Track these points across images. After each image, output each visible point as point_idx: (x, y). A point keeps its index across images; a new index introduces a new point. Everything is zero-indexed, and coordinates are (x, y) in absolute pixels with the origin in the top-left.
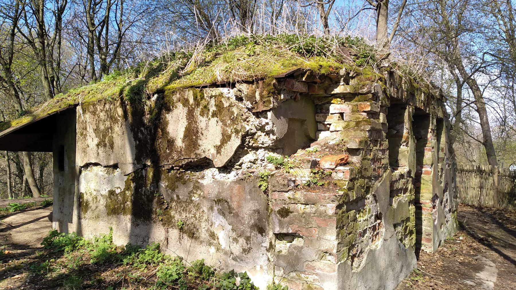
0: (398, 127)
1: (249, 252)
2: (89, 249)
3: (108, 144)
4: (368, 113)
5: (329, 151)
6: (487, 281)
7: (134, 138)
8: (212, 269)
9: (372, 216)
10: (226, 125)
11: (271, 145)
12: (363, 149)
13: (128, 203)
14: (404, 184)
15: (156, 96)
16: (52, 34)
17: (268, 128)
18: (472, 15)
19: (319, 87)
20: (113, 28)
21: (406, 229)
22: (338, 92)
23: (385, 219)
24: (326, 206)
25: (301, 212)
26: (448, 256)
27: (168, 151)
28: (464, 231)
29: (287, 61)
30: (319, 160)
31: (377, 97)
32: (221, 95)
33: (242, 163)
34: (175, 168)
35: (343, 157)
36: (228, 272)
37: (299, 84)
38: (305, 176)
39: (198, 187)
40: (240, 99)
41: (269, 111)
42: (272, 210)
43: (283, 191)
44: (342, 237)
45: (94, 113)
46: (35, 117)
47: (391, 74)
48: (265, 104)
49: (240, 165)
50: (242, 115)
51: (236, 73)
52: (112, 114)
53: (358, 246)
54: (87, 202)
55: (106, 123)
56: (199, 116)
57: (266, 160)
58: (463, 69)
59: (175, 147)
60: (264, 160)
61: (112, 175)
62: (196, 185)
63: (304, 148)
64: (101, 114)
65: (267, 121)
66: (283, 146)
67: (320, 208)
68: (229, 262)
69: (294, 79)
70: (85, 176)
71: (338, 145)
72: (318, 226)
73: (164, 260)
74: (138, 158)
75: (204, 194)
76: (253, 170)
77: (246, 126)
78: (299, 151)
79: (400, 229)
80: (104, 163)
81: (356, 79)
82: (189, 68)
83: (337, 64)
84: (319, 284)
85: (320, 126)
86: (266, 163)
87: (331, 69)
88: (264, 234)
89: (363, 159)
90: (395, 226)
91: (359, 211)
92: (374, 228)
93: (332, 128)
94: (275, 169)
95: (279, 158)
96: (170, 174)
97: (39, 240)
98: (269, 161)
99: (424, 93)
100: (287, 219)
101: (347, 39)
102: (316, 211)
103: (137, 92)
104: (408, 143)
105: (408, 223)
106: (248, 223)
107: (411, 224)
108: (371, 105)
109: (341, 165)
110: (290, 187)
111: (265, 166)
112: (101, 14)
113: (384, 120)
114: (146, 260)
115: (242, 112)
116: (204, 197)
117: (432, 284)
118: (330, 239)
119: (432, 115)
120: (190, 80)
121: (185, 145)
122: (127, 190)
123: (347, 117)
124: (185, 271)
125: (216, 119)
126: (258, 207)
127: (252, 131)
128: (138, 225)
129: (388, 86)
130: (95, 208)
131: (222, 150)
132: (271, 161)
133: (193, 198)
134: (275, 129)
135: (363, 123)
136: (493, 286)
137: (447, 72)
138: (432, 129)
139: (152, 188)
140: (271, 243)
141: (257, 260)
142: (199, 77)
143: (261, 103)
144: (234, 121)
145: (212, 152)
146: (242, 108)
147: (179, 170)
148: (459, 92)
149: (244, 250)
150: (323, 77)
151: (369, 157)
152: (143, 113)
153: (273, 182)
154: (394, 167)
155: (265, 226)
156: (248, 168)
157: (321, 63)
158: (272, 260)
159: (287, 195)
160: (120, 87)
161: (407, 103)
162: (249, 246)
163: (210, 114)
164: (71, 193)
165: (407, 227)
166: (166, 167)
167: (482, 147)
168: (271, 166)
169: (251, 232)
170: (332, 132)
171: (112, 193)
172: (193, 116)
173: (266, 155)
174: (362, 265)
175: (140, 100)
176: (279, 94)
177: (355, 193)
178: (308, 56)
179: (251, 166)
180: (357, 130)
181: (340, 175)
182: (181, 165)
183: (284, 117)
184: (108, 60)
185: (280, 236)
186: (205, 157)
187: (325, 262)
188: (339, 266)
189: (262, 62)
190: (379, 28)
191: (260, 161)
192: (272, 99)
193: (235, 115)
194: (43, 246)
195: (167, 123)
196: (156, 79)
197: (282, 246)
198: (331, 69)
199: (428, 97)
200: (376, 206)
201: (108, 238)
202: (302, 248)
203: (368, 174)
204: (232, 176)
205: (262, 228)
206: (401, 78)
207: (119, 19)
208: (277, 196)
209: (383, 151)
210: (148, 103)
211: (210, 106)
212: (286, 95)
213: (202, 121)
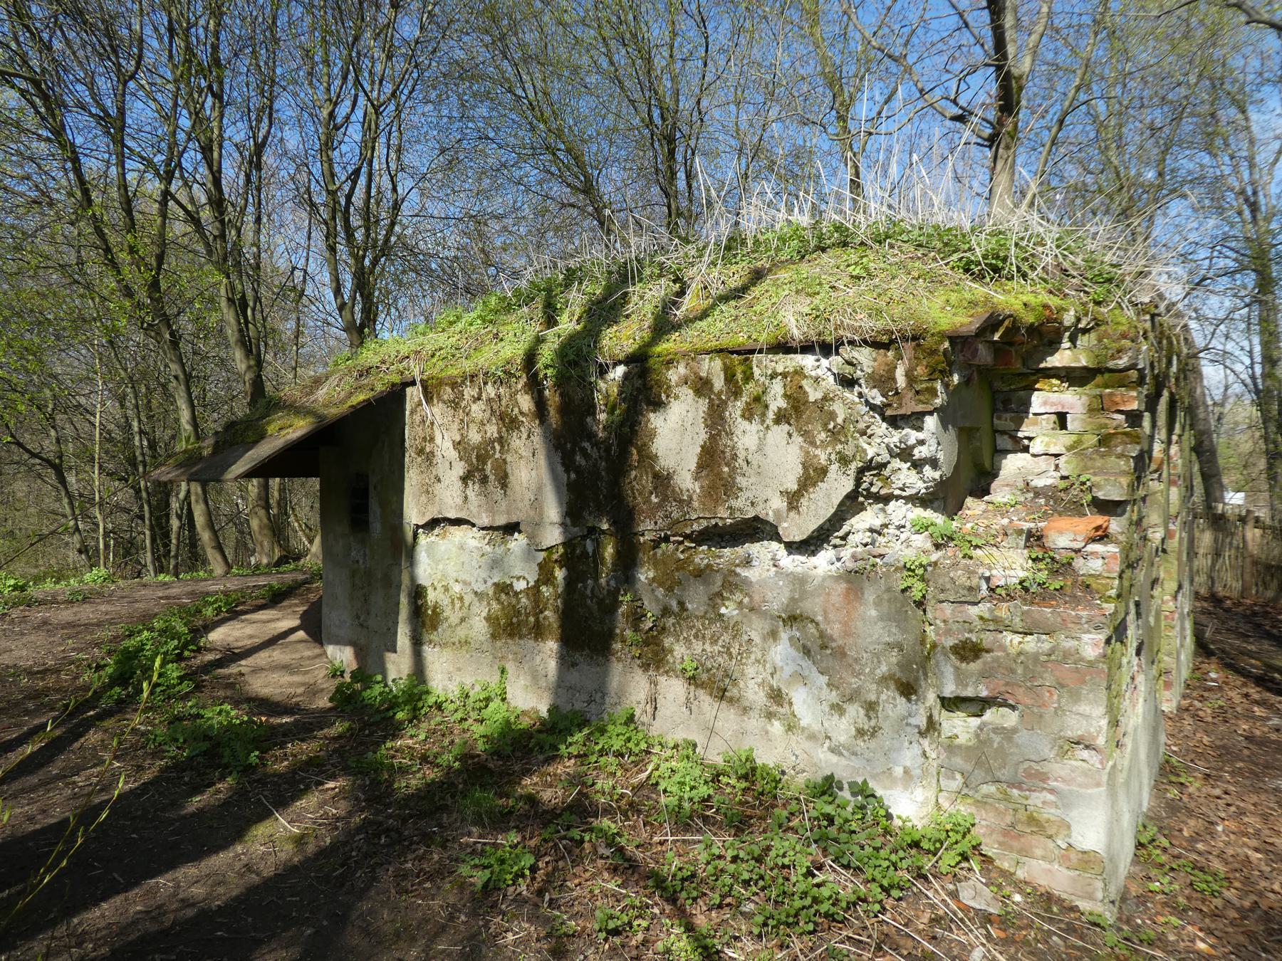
1: (873, 735)
3: (492, 478)
7: (563, 464)
10: (813, 443)
11: (923, 491)
15: (620, 370)
17: (919, 453)
24: (1079, 639)
25: (1013, 651)
26: (1210, 719)
27: (654, 499)
32: (799, 372)
33: (848, 534)
34: (672, 539)
39: (732, 583)
40: (848, 382)
41: (931, 413)
45: (455, 404)
49: (844, 538)
54: (435, 607)
55: (488, 427)
56: (740, 420)
57: (908, 525)
59: (673, 491)
61: (503, 547)
62: (731, 579)
64: (474, 407)
65: (921, 436)
67: (1064, 644)
68: (822, 756)
70: (431, 546)
72: (1059, 684)
74: (573, 513)
76: (881, 551)
80: (485, 520)
81: (1093, 335)
82: (690, 303)
84: (1058, 812)
85: (1003, 442)
88: (914, 697)
93: (1036, 447)
96: (659, 552)
100: (975, 666)
103: (578, 358)
106: (872, 672)
116: (752, 610)
121: (702, 487)
122: (545, 583)
123: (1076, 423)
125: (786, 427)
126: (899, 638)
127: (879, 459)
128: (574, 665)
130: (457, 621)
131: (804, 501)
132: (923, 528)
133: (723, 610)
134: (940, 456)
139: (613, 583)
140: (930, 718)
141: (895, 755)
142: (724, 327)
143: (911, 394)
144: (836, 435)
145: (774, 506)
146: (853, 403)
147: (682, 543)
149: (860, 733)
150: (1032, 329)
152: (591, 409)
153: (941, 581)
155: (917, 679)
158: (934, 755)
159: (974, 611)
162: (873, 723)
163: (771, 415)
164: (391, 585)
168: (921, 541)
169: (879, 693)
171: (503, 588)
172: (722, 418)
173: (911, 516)
181: (1096, 565)
182: (688, 532)
185: (951, 704)
186: (756, 518)
187: (1073, 762)
189: (897, 294)
191: (901, 531)
193: (840, 420)
195: (652, 434)
196: (615, 328)
197: (960, 726)
202: (1014, 730)
204: (823, 562)
210: (602, 384)
211: (768, 398)
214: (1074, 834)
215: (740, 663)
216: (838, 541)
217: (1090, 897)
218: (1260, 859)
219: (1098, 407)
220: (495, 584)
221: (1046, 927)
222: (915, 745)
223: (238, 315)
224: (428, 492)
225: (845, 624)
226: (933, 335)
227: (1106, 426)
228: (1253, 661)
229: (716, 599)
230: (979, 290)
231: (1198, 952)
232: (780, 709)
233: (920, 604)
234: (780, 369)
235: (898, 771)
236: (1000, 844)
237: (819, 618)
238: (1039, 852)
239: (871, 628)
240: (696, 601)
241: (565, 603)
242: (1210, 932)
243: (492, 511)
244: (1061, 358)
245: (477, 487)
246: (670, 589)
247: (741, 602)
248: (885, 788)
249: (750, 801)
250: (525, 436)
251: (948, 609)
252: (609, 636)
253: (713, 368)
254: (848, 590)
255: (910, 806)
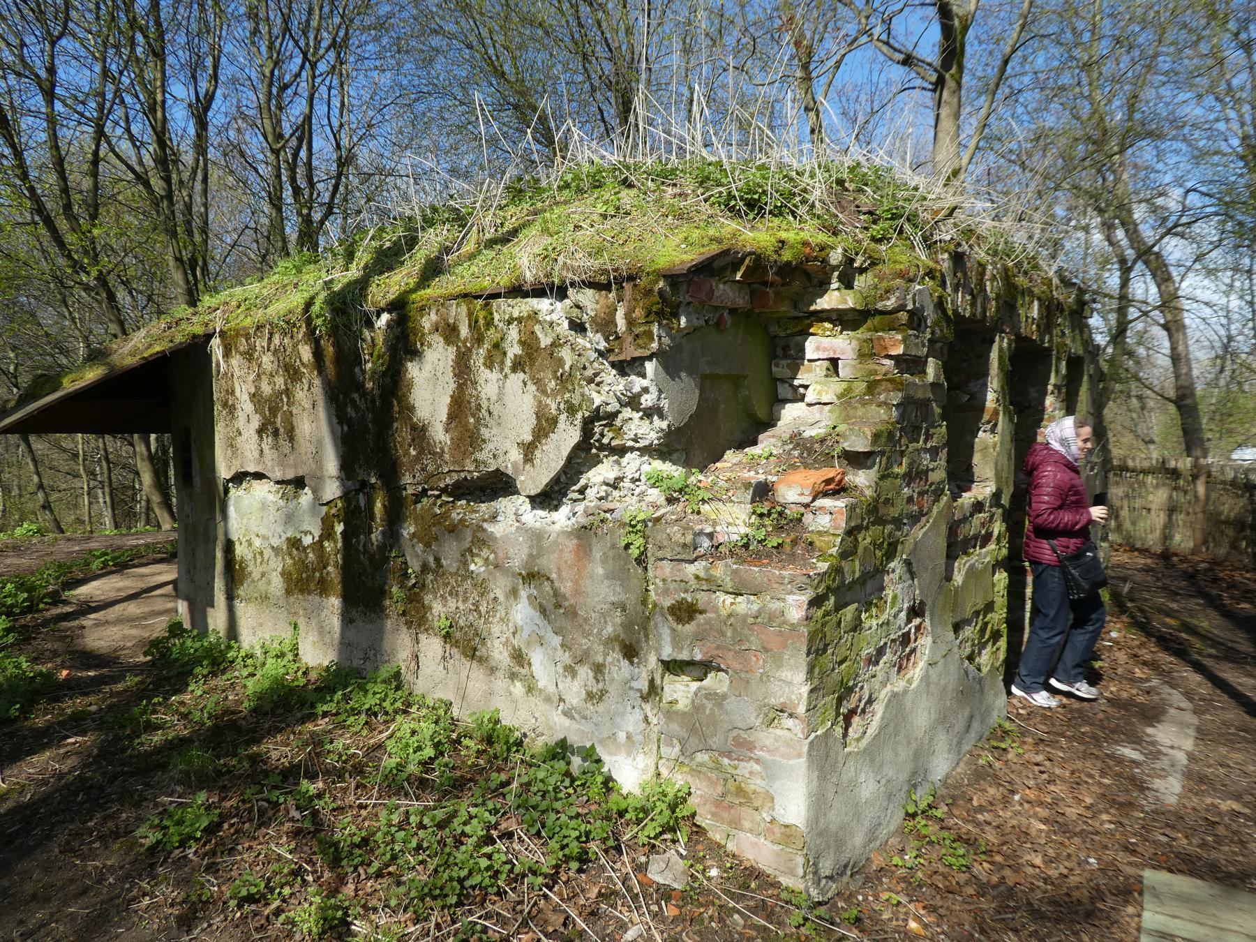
0: (973, 386)
1: (600, 699)
2: (245, 673)
3: (282, 430)
4: (898, 359)
5: (801, 455)
6: (1172, 747)
8: (517, 734)
9: (900, 611)
10: (544, 392)
11: (656, 442)
12: (882, 453)
13: (330, 569)
14: (983, 524)
15: (385, 317)
16: (188, 158)
17: (647, 400)
18: (1161, 98)
19: (777, 294)
20: (322, 144)
21: (983, 631)
22: (827, 307)
23: (932, 615)
25: (724, 613)
27: (413, 452)
28: (1125, 618)
29: (697, 231)
30: (775, 479)
31: (920, 320)
33: (585, 487)
34: (430, 493)
35: (831, 475)
36: (552, 742)
37: (726, 287)
38: (737, 522)
39: (481, 540)
40: (578, 327)
41: (650, 358)
42: (655, 605)
43: (683, 560)
44: (822, 673)
45: (249, 356)
46: (112, 368)
47: (958, 259)
48: (640, 342)
49: (582, 491)
50: (585, 368)
51: (569, 261)
52: (287, 359)
53: (862, 688)
54: (241, 562)
55: (276, 379)
58: (1136, 231)
59: (428, 443)
60: (639, 480)
61: (295, 501)
62: (479, 534)
63: (740, 446)
65: (645, 383)
66: (691, 444)
67: (771, 605)
68: (556, 719)
69: (713, 275)
71: (823, 441)
72: (764, 648)
73: (409, 705)
74: (347, 467)
75: (496, 558)
76: (611, 506)
77: (594, 395)
78: (729, 454)
79: (968, 632)
80: (278, 475)
81: (870, 274)
83: (822, 238)
85: (783, 391)
86: (644, 488)
87: (808, 250)
88: (636, 660)
89: (882, 478)
90: (957, 628)
91: (868, 606)
92: (905, 639)
94: (664, 503)
95: (676, 474)
96: (419, 506)
97: (141, 642)
98: (653, 481)
99: (1039, 299)
100: (689, 628)
101: (852, 170)
102: (760, 612)
103: (346, 307)
104: (995, 425)
105: (989, 616)
106: (599, 633)
107: (998, 617)
108: (904, 340)
109: (825, 494)
110: (701, 551)
111: (643, 494)
112: (296, 111)
113: (936, 375)
114: (367, 706)
115: (583, 359)
116: (496, 566)
117: (1040, 758)
118: (792, 682)
119: (1058, 352)
120: (463, 277)
121: (452, 439)
123: (847, 369)
124: (454, 736)
125: (521, 376)
126: (623, 597)
127: (609, 409)
128: (351, 621)
129: (949, 290)
130: (259, 576)
131: (538, 453)
132: (656, 482)
133: (472, 567)
134: (665, 404)
135: (884, 385)
136: (1185, 762)
137: (1097, 237)
138: (1055, 386)
141: (618, 720)
143: (630, 339)
144: (565, 381)
145: (512, 459)
146: (585, 349)
147: (439, 497)
148: (1125, 282)
149: (590, 696)
150: (786, 270)
151: (896, 470)
152: (357, 360)
153: (659, 538)
154: (961, 484)
155: (638, 641)
156: (601, 499)
157: (783, 235)
159: (691, 569)
160: (306, 295)
161: (997, 328)
162: (601, 685)
164: (210, 539)
165: (986, 624)
166: (410, 491)
167: (1172, 408)
168: (655, 495)
169: (606, 655)
170: (810, 405)
171: (295, 543)
174: (872, 731)
175: (348, 327)
176: (676, 316)
177: (857, 563)
178: (751, 216)
179: (607, 495)
180: (871, 402)
181: (824, 521)
182: (442, 485)
183: (690, 374)
184: (317, 216)
185: (673, 667)
186: (498, 470)
187: (778, 732)
188: (811, 743)
190: (940, 135)
191: (633, 483)
192: (655, 328)
193: (567, 368)
194: (149, 658)
195: (410, 385)
197: (680, 690)
198: (808, 250)
199: (1048, 308)
200: (910, 586)
201: (286, 648)
203: (894, 512)
204: (562, 518)
205: (631, 645)
206: (982, 266)
207: (336, 123)
208: (668, 570)
209: (934, 452)
210: (367, 334)
211: (505, 345)
212: (694, 317)
213: (488, 383)
214: (777, 807)
215: (487, 622)
216: (576, 496)
217: (792, 873)
218: (1041, 831)
219: (867, 353)
220: (288, 539)
221: (732, 904)
222: (637, 710)
223: (186, 274)
224: (232, 446)
225: (576, 582)
226: (648, 274)
227: (875, 372)
228: (1168, 620)
229: (467, 555)
230: (729, 226)
231: (907, 934)
232: (521, 670)
233: (641, 561)
234: (516, 315)
235: (622, 736)
236: (713, 815)
237: (554, 576)
238: (747, 824)
239: (599, 590)
240: (450, 554)
241: (344, 558)
242: (932, 909)
243: (282, 464)
244: (832, 299)
245: (270, 439)
246: (428, 545)
247: (487, 559)
248: (611, 754)
249: (478, 765)
250: (306, 388)
251: (667, 568)
252: (382, 593)
253: (459, 313)
254: (578, 545)
255: (631, 774)
